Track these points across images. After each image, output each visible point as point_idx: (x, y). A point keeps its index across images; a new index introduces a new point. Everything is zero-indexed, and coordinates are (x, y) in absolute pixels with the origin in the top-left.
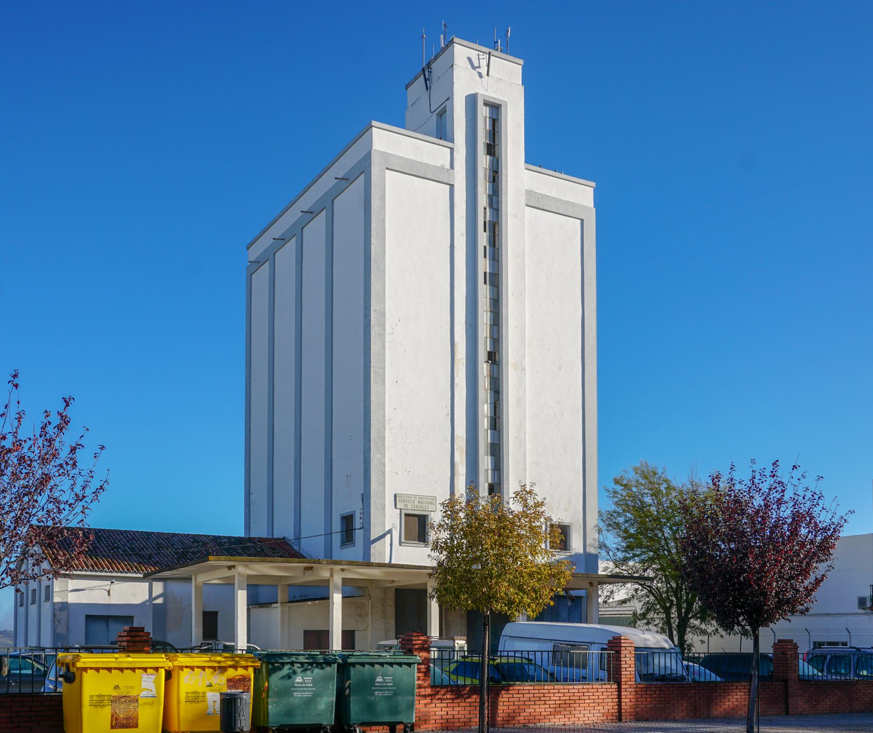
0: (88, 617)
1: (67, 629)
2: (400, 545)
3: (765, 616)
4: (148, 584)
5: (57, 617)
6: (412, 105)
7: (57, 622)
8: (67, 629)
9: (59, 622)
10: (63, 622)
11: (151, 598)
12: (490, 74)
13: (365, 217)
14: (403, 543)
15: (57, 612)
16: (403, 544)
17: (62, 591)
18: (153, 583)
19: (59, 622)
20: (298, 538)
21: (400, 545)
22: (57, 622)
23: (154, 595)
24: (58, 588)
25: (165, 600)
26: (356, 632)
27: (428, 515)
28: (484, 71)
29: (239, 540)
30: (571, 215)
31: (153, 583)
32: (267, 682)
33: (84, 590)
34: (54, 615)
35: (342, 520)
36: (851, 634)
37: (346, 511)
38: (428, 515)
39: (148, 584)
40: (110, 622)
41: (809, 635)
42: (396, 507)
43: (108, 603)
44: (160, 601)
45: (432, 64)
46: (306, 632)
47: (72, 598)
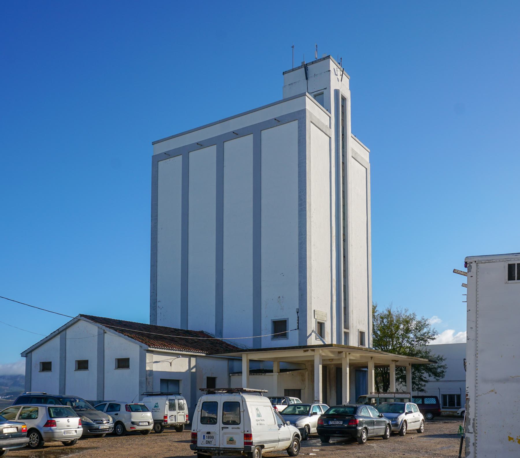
0: (162, 381)
1: (153, 388)
2: (316, 340)
3: (387, 383)
4: (188, 359)
5: (148, 380)
6: (289, 85)
7: (148, 384)
8: (153, 388)
9: (149, 383)
10: (151, 383)
11: (190, 369)
12: (286, 75)
13: (299, 146)
14: (317, 338)
15: (148, 377)
16: (317, 339)
17: (150, 363)
18: (191, 358)
19: (149, 383)
20: (220, 332)
21: (316, 340)
22: (148, 384)
23: (191, 367)
24: (149, 360)
25: (196, 370)
26: (301, 390)
27: (324, 323)
28: (340, 79)
29: (175, 331)
30: (363, 165)
31: (191, 358)
32: (13, 430)
33: (159, 362)
34: (146, 378)
35: (273, 323)
36: (440, 391)
37: (280, 317)
38: (324, 323)
39: (188, 359)
40: (169, 383)
41: (461, 391)
42: (82, 315)
43: (170, 371)
44: (194, 370)
45: (309, 65)
46: (285, 390)
47: (156, 368)
